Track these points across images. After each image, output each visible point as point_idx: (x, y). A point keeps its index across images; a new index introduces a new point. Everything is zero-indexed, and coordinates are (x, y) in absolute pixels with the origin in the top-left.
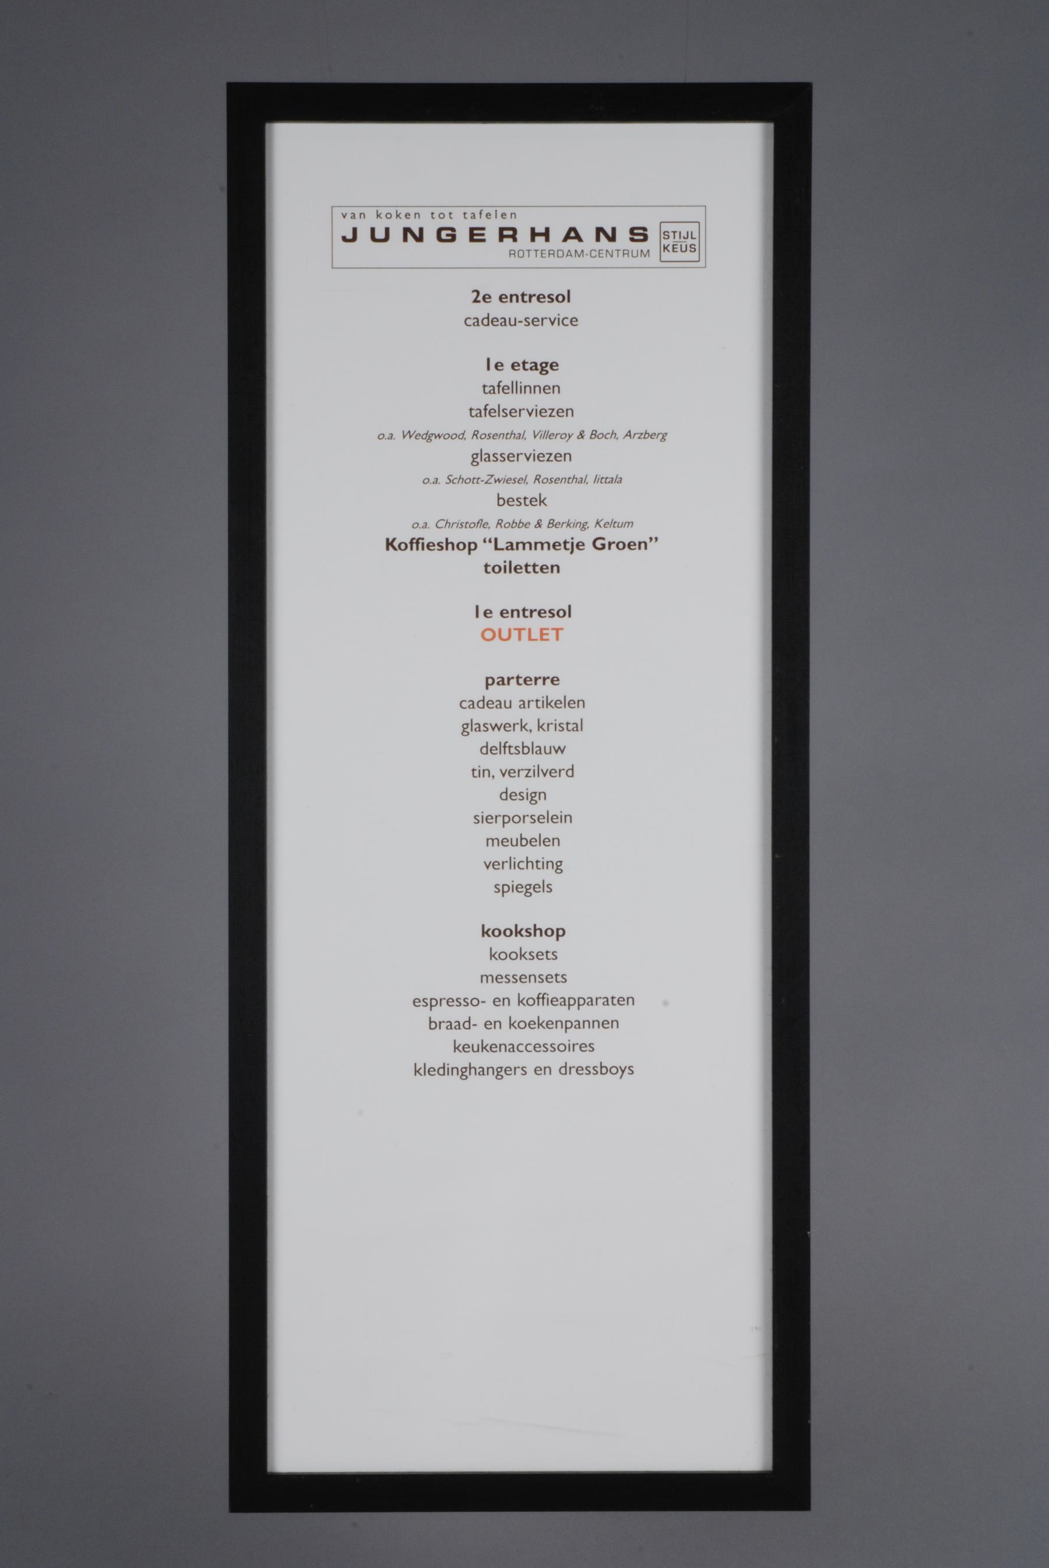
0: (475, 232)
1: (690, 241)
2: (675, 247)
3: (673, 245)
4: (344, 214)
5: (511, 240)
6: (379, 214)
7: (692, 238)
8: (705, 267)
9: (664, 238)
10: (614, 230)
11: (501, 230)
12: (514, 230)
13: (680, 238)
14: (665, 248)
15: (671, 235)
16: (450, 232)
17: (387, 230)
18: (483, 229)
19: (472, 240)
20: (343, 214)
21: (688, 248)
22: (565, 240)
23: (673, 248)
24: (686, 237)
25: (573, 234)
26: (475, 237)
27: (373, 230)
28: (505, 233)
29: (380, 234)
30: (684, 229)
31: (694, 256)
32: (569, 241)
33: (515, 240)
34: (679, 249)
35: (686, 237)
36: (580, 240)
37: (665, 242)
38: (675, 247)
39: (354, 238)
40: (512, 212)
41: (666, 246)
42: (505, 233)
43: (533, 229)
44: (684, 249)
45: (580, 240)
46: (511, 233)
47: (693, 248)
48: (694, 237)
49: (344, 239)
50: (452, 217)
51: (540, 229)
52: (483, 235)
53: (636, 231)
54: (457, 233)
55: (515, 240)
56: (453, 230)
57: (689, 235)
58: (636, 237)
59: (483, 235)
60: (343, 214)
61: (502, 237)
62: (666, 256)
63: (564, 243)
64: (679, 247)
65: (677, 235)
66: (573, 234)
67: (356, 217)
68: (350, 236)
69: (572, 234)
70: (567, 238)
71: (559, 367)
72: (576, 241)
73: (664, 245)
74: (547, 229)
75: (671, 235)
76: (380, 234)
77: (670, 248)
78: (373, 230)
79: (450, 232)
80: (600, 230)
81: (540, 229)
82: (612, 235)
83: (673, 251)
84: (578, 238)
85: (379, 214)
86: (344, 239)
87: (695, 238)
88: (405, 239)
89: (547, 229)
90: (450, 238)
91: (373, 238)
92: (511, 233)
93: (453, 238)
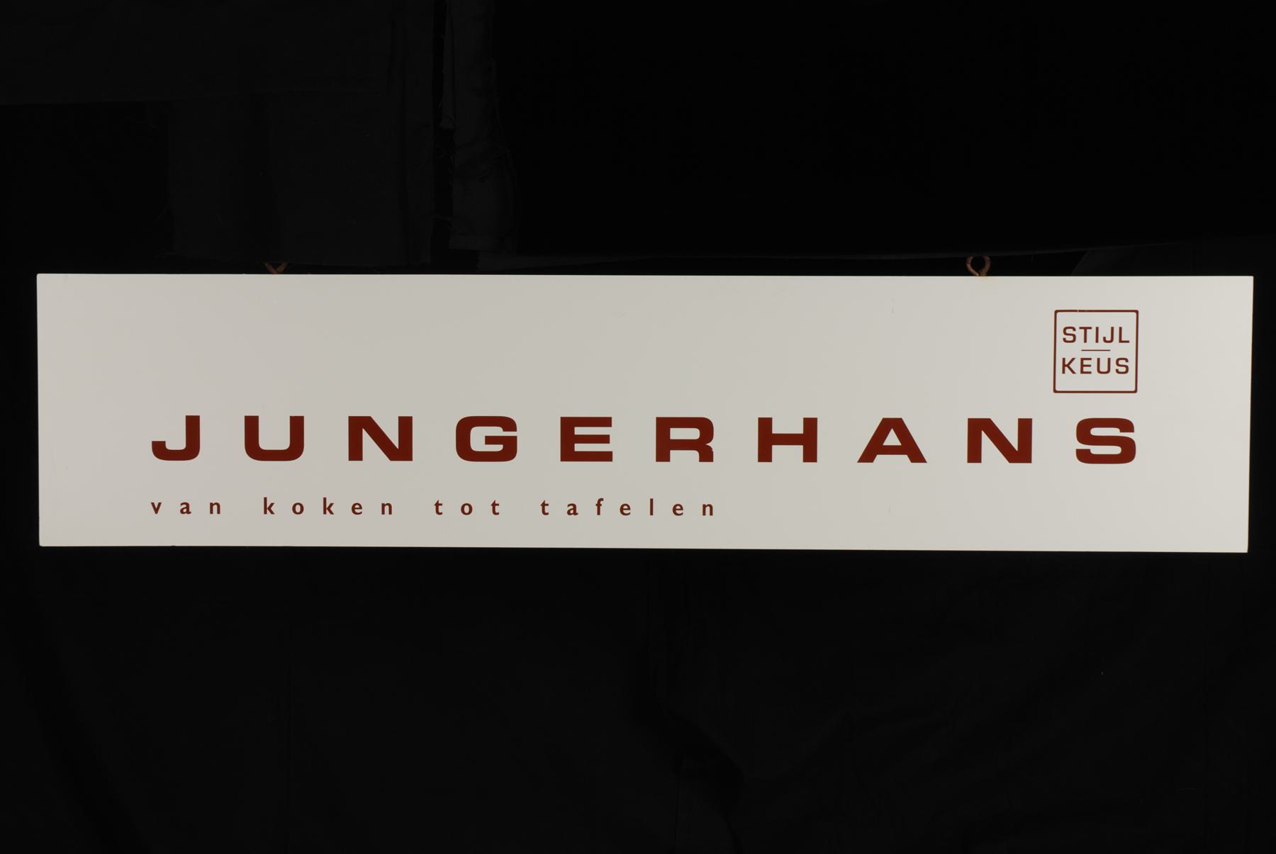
0: (579, 431)
1: (1117, 350)
2: (1086, 362)
3: (1082, 360)
5: (695, 454)
7: (1121, 341)
8: (1135, 391)
11: (664, 425)
12: (705, 427)
14: (1065, 365)
15: (1080, 334)
16: (497, 431)
17: (297, 425)
18: (606, 422)
19: (568, 454)
21: (1114, 366)
22: (868, 456)
23: (1082, 366)
24: (1108, 338)
25: (892, 439)
26: (579, 447)
27: (252, 424)
28: (676, 434)
29: (274, 436)
30: (1105, 323)
31: (1127, 382)
32: (880, 458)
33: (707, 456)
34: (1094, 369)
35: (1108, 338)
36: (917, 456)
37: (1066, 351)
38: (1086, 362)
39: (192, 450)
42: (676, 434)
43: (765, 424)
44: (1104, 368)
45: (917, 456)
46: (693, 434)
47: (1122, 366)
49: (160, 450)
51: (790, 455)
52: (605, 439)
53: (1096, 432)
54: (521, 435)
55: (707, 456)
56: (508, 424)
57: (1117, 335)
58: (1096, 450)
59: (605, 439)
61: (664, 449)
62: (1066, 380)
64: (1094, 363)
65: (1091, 334)
66: (892, 439)
68: (177, 442)
70: (874, 450)
72: (905, 458)
73: (1064, 360)
74: (811, 424)
75: (1080, 334)
76: (274, 436)
77: (1076, 366)
78: (252, 424)
79: (497, 431)
80: (979, 428)
83: (1082, 372)
84: (911, 450)
86: (160, 450)
88: (405, 425)
89: (811, 424)
90: (498, 448)
91: (254, 449)
92: (693, 434)
93: (508, 450)
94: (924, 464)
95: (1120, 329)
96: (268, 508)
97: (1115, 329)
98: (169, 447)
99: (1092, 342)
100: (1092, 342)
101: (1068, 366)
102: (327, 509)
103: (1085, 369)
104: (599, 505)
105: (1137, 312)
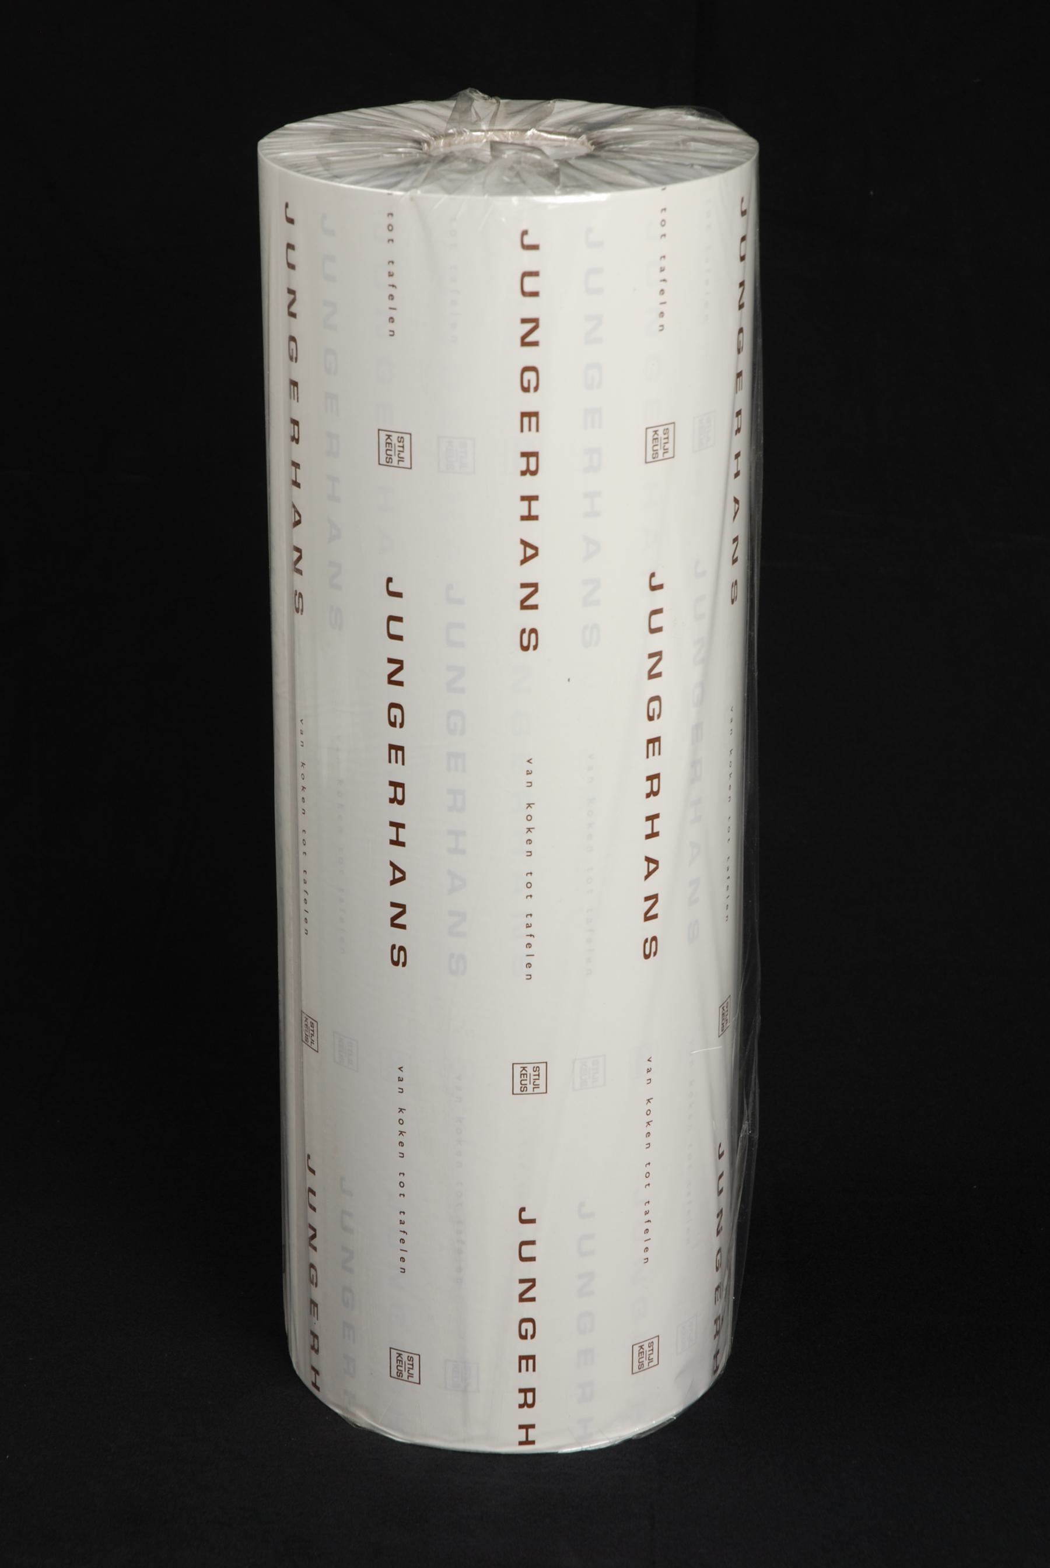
2: (525, 1076)
4: (531, 761)
6: (531, 830)
9: (526, 1091)
10: (535, 607)
12: (534, 473)
13: (534, 1079)
16: (533, 384)
17: (535, 294)
20: (531, 759)
23: (524, 1074)
24: (535, 1083)
27: (535, 274)
28: (533, 460)
35: (535, 1083)
36: (523, 562)
38: (525, 1076)
39: (522, 1221)
40: (533, 783)
41: (526, 1069)
45: (523, 562)
48: (535, 1089)
49: (523, 1210)
50: (528, 916)
54: (532, 393)
60: (531, 759)
63: (519, 541)
66: (530, 552)
67: (528, 928)
68: (525, 1216)
69: (530, 551)
71: (528, 949)
72: (522, 557)
73: (526, 1067)
78: (535, 274)
81: (536, 508)
82: (533, 587)
85: (531, 830)
87: (398, 463)
93: (523, 1337)
94: (647, 856)
95: (522, 431)
96: (529, 805)
97: (395, 761)
98: (523, 1213)
99: (398, 449)
100: (398, 449)
101: (529, 806)
102: (529, 830)
103: (522, 1076)
104: (531, 935)
105: (379, 464)
